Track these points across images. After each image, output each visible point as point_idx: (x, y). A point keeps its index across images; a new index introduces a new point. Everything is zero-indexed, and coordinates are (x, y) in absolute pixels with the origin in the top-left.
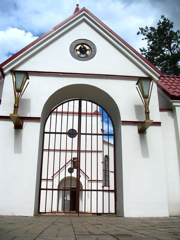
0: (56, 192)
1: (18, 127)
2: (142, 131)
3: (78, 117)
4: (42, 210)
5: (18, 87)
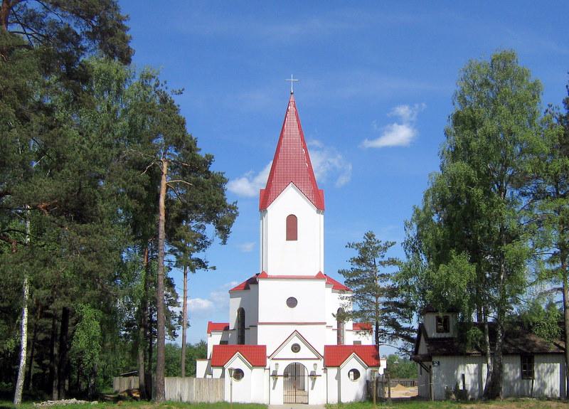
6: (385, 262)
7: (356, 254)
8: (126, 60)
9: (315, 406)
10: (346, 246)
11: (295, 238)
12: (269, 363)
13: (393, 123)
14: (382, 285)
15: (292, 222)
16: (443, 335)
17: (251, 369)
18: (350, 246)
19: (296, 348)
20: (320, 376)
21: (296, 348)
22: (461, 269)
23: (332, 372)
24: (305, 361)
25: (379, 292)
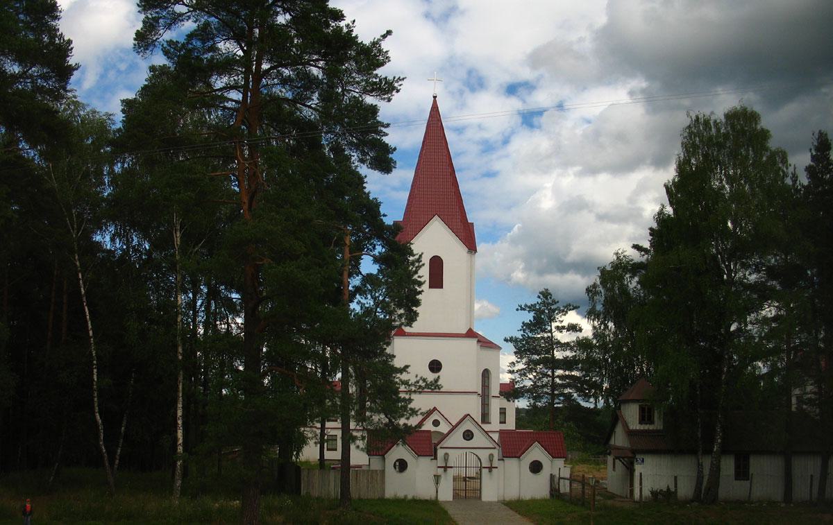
6: (563, 328)
7: (529, 317)
8: (581, 330)
9: (529, 500)
10: (517, 310)
12: (441, 453)
14: (559, 355)
16: (646, 427)
17: (416, 459)
23: (511, 463)
24: (477, 450)
25: (554, 364)
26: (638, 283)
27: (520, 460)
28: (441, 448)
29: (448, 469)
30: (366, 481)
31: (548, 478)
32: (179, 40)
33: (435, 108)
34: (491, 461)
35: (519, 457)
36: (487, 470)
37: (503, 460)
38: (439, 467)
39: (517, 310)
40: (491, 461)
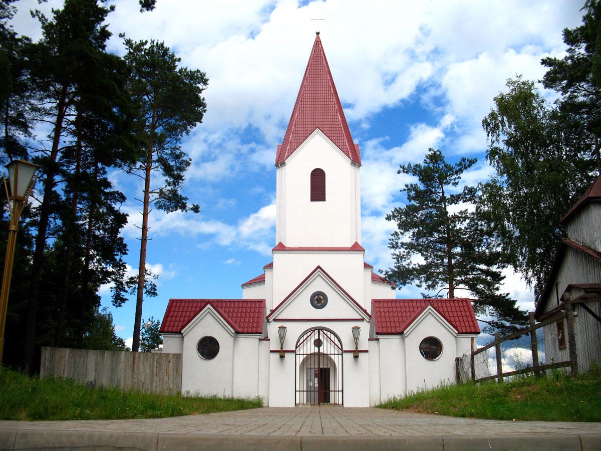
0: (305, 393)
1: (282, 357)
2: (356, 357)
3: (320, 351)
4: (298, 402)
5: (282, 336)
11: (322, 198)
12: (273, 329)
13: (100, 8)
15: (318, 180)
18: (505, 277)
19: (319, 300)
20: (367, 351)
21: (319, 300)
22: (423, 31)
23: (390, 343)
26: (526, 189)
27: (403, 339)
28: (275, 320)
29: (286, 355)
30: (148, 371)
31: (453, 363)
32: (106, 48)
33: (318, 43)
34: (356, 338)
35: (401, 333)
36: (352, 355)
37: (378, 340)
38: (271, 351)
39: (399, 172)
40: (356, 338)
